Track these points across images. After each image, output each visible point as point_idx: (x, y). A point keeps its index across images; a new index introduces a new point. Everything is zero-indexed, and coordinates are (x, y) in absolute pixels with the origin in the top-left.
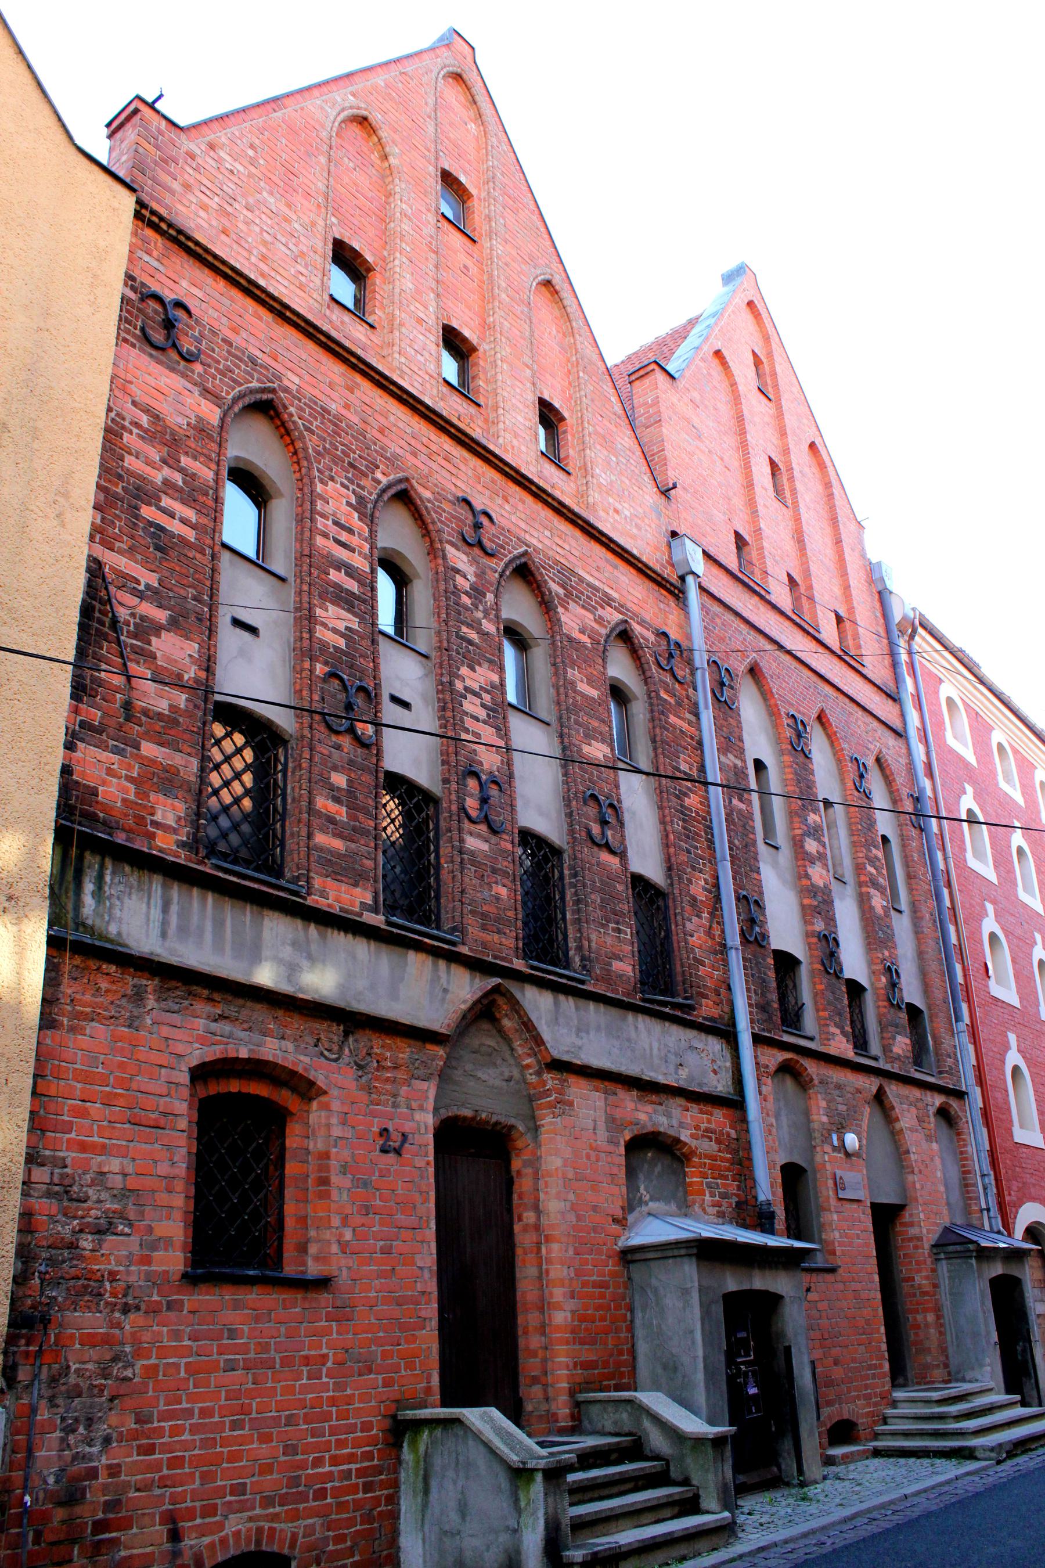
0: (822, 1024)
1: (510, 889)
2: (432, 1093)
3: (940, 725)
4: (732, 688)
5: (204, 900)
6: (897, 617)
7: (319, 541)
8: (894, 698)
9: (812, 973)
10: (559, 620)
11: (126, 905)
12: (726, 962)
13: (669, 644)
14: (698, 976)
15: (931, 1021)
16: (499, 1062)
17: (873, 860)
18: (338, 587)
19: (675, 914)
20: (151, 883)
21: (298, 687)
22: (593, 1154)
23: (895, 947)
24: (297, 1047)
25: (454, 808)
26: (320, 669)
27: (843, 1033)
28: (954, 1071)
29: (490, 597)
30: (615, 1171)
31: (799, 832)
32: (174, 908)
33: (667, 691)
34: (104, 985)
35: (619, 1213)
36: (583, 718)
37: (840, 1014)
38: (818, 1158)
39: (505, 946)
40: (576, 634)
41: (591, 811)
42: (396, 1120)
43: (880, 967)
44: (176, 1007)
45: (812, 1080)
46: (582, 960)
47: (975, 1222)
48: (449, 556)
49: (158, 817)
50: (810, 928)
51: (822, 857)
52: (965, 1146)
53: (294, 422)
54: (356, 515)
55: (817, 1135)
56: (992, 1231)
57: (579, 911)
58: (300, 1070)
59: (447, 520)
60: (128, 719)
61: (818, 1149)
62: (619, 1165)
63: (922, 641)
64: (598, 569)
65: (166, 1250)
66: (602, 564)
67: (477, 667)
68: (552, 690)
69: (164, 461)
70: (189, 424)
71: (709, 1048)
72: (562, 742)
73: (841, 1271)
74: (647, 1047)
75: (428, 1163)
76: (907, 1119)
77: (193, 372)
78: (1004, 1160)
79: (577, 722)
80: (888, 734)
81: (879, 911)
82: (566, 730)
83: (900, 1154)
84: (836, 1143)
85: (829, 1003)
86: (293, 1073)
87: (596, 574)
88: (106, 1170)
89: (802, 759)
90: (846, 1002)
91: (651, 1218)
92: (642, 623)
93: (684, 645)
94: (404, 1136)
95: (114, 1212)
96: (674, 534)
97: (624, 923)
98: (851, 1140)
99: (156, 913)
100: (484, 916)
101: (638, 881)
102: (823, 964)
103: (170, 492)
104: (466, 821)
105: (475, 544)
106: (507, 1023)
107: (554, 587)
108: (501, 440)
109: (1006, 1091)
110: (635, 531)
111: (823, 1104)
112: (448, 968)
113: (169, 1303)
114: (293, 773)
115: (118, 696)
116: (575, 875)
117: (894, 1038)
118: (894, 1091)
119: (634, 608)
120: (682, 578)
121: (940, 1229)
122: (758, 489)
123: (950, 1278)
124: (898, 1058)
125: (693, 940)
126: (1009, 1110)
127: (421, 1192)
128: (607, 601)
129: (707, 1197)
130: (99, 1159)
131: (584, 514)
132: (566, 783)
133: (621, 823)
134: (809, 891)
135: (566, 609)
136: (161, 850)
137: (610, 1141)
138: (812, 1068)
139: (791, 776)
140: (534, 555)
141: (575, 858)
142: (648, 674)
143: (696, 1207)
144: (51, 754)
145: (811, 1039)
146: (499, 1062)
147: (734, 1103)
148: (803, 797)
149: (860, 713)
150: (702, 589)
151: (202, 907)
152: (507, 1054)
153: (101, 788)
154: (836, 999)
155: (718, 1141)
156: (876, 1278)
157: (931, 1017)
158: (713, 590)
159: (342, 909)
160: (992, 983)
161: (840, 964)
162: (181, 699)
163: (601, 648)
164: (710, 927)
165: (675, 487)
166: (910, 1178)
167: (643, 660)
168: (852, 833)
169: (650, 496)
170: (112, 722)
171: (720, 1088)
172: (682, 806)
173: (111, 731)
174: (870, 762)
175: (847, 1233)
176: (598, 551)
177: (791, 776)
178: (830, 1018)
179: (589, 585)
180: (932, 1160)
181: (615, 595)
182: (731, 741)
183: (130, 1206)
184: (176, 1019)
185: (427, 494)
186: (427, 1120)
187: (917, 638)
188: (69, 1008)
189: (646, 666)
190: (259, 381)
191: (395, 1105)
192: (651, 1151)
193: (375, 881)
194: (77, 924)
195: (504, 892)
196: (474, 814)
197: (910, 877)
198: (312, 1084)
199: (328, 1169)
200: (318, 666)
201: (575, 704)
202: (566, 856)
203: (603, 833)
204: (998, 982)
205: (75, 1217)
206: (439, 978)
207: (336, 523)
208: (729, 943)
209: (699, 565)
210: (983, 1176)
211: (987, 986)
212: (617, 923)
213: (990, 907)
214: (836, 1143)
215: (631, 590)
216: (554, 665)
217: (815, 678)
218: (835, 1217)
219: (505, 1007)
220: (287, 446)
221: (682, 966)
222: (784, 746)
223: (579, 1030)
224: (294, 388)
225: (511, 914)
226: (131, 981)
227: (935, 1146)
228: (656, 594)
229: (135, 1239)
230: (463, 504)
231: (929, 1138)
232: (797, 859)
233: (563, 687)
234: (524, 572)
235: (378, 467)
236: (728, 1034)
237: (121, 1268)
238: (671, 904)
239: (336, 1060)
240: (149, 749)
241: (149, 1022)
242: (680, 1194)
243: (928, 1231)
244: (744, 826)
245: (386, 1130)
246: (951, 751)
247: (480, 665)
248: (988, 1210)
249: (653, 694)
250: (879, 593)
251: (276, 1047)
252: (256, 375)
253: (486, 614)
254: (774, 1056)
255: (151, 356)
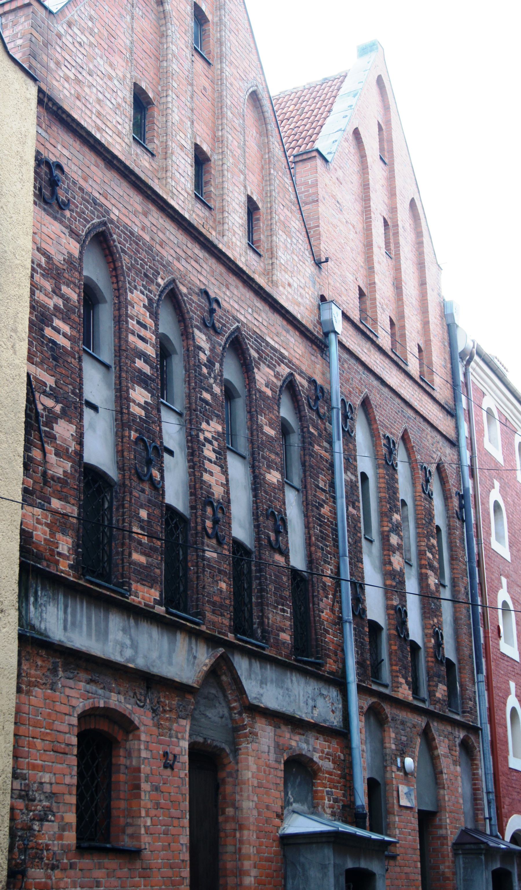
0: (394, 676)
1: (227, 584)
2: (188, 728)
3: (481, 432)
4: (352, 419)
5: (82, 602)
6: (460, 349)
7: (131, 338)
8: (451, 413)
9: (389, 637)
10: (254, 378)
11: (48, 610)
12: (342, 631)
13: (316, 389)
14: (326, 642)
15: (460, 672)
16: (217, 705)
17: (430, 548)
18: (140, 371)
19: (313, 596)
20: (58, 594)
21: (120, 448)
22: (267, 769)
23: (441, 616)
24: (125, 698)
25: (199, 528)
26: (134, 435)
27: (407, 682)
28: (472, 712)
29: (217, 365)
30: (278, 782)
31: (386, 529)
32: (69, 610)
33: (314, 426)
34: (40, 663)
35: (279, 810)
36: (267, 453)
37: (405, 668)
38: (388, 775)
39: (220, 622)
40: (264, 389)
41: (270, 523)
42: (171, 746)
43: (430, 631)
44: (71, 675)
45: (387, 717)
46: (262, 632)
47: (481, 828)
48: (196, 337)
49: (60, 550)
50: (390, 602)
51: (400, 547)
52: (477, 769)
53: (116, 246)
54: (148, 314)
55: (388, 758)
56: (491, 835)
57: (262, 597)
58: (127, 713)
59: (195, 307)
60: (45, 484)
61: (388, 768)
62: (281, 777)
63: (477, 368)
64: (277, 334)
65: (69, 831)
66: (280, 330)
67: (210, 421)
68: (247, 432)
69: (54, 291)
70: (64, 260)
71: (330, 694)
72: (253, 472)
73: (399, 858)
74: (297, 694)
75: (186, 775)
76: (442, 749)
77: (65, 217)
78: (502, 779)
79: (263, 457)
80: (446, 444)
81: (433, 587)
82: (257, 464)
83: (437, 773)
84: (399, 764)
85: (400, 660)
86: (123, 716)
87: (276, 339)
88: (43, 781)
89: (391, 471)
90: (409, 659)
91: (295, 815)
92: (301, 373)
93: (326, 387)
94: (175, 756)
95: (47, 807)
96: (323, 299)
97: (287, 605)
98: (409, 762)
99: (61, 614)
100: (214, 604)
101: (295, 572)
102: (397, 631)
103: (57, 314)
104: (206, 537)
105: (210, 327)
106: (224, 678)
107: (254, 354)
108: (225, 238)
109: (506, 727)
110: (300, 299)
111: (393, 735)
112: (196, 641)
113: (71, 864)
114: (117, 509)
115: (40, 468)
116: (260, 571)
117: (437, 686)
118: (435, 726)
119: (297, 362)
120: (326, 335)
121: (458, 832)
122: (375, 249)
123: (464, 868)
124: (439, 701)
125: (323, 615)
126: (507, 742)
127: (182, 794)
128: (282, 359)
129: (326, 801)
130: (40, 774)
131: (268, 289)
132: (255, 502)
133: (287, 533)
134: (391, 574)
135: (259, 369)
136: (62, 572)
137: (276, 761)
138: (388, 710)
139: (383, 485)
140: (242, 328)
141: (260, 559)
142: (303, 413)
143: (320, 808)
144: (15, 514)
145: (386, 686)
146: (217, 705)
147: (342, 734)
148: (391, 502)
149: (429, 429)
150: (341, 344)
151: (82, 612)
152: (221, 699)
153: (34, 533)
154: (403, 656)
155: (334, 762)
156: (419, 864)
157: (460, 669)
158: (347, 344)
159: (146, 605)
160: (502, 641)
161: (407, 630)
162: (68, 465)
163: (277, 398)
164: (333, 605)
165: (327, 260)
166: (442, 792)
167: (300, 403)
168: (417, 527)
169: (309, 268)
170: (37, 487)
171: (335, 724)
172: (320, 515)
173: (38, 493)
174: (433, 468)
175: (404, 833)
176: (277, 320)
177: (383, 485)
178: (400, 671)
179: (273, 348)
180: (456, 779)
181: (286, 353)
182: (350, 463)
183: (54, 804)
184: (71, 683)
185: (184, 290)
186: (185, 744)
187: (472, 364)
188: (25, 679)
189: (302, 408)
190: (98, 217)
191: (170, 737)
192: (298, 769)
193: (161, 584)
194: (27, 625)
195: (223, 586)
196: (210, 531)
197: (453, 558)
198: (132, 722)
199: (139, 778)
200: (133, 433)
201: (262, 443)
202: (253, 556)
203: (277, 540)
204: (506, 642)
205: (31, 811)
206: (192, 648)
207: (139, 323)
208: (345, 618)
209: (339, 325)
210: (488, 793)
211: (498, 644)
212: (283, 605)
213: (504, 580)
214: (399, 764)
215: (296, 348)
216: (249, 412)
217: (402, 405)
218: (397, 819)
219: (224, 668)
220: (109, 263)
221: (316, 634)
222: (381, 462)
223: (262, 683)
224: (115, 218)
225: (227, 602)
226: (51, 660)
227: (458, 768)
228: (310, 349)
229: (56, 824)
230: (204, 296)
231: (455, 763)
232: (383, 549)
233: (254, 429)
234: (237, 345)
235: (159, 274)
236: (339, 682)
237: (51, 842)
238: (310, 589)
239: (142, 707)
240: (56, 504)
241: (60, 686)
242: (310, 798)
243: (452, 833)
244: (355, 527)
245: (167, 753)
246: (487, 453)
247: (212, 420)
248: (490, 819)
249: (305, 429)
250: (448, 325)
251: (116, 699)
252: (96, 213)
253: (215, 378)
254: (366, 700)
255: (45, 210)
